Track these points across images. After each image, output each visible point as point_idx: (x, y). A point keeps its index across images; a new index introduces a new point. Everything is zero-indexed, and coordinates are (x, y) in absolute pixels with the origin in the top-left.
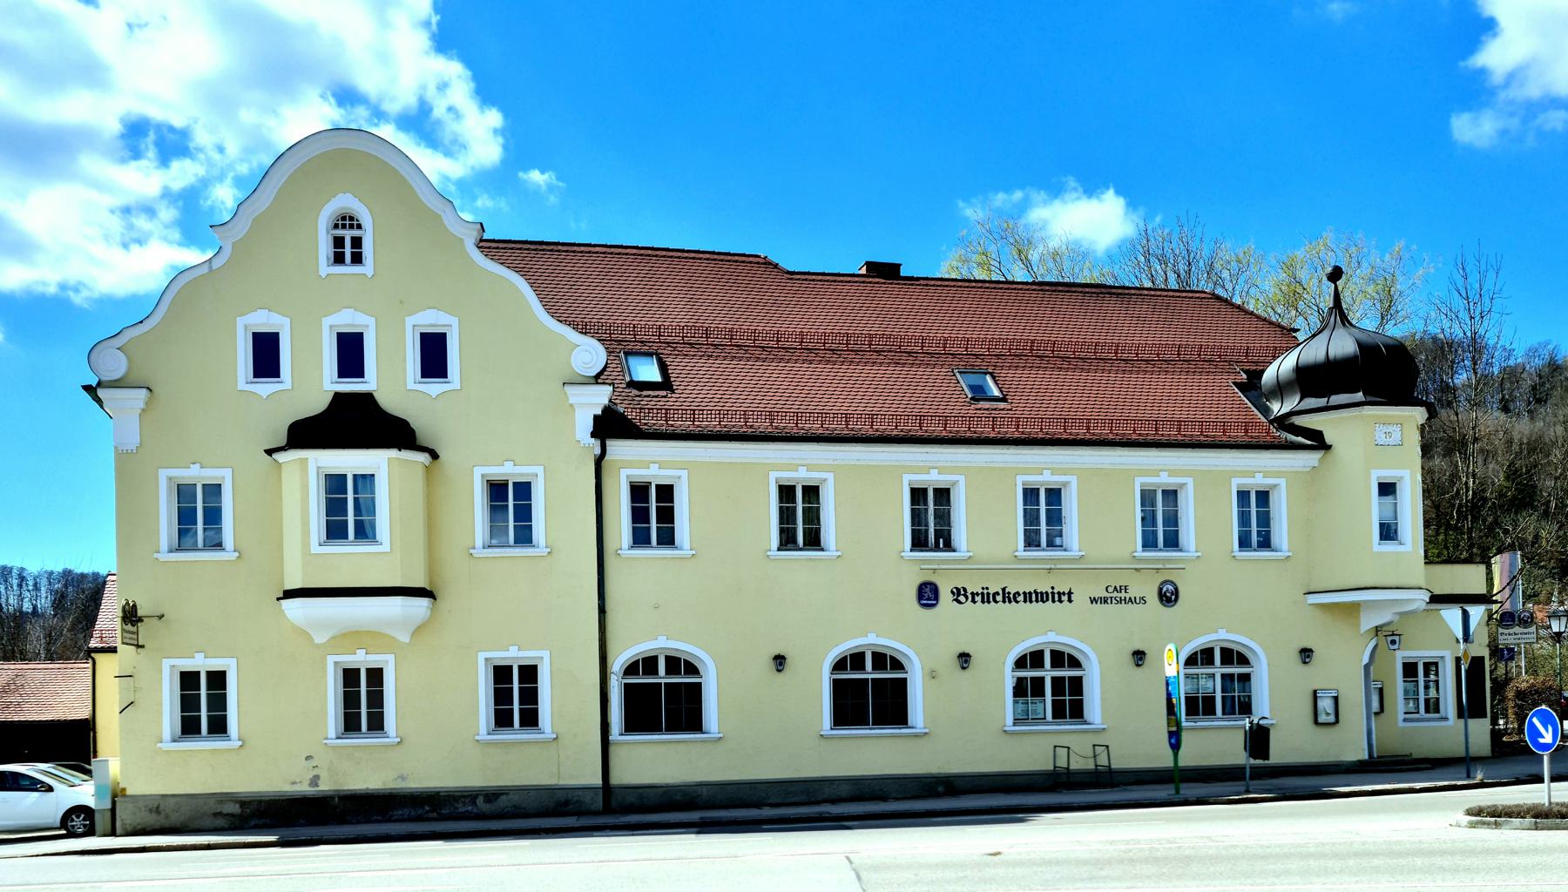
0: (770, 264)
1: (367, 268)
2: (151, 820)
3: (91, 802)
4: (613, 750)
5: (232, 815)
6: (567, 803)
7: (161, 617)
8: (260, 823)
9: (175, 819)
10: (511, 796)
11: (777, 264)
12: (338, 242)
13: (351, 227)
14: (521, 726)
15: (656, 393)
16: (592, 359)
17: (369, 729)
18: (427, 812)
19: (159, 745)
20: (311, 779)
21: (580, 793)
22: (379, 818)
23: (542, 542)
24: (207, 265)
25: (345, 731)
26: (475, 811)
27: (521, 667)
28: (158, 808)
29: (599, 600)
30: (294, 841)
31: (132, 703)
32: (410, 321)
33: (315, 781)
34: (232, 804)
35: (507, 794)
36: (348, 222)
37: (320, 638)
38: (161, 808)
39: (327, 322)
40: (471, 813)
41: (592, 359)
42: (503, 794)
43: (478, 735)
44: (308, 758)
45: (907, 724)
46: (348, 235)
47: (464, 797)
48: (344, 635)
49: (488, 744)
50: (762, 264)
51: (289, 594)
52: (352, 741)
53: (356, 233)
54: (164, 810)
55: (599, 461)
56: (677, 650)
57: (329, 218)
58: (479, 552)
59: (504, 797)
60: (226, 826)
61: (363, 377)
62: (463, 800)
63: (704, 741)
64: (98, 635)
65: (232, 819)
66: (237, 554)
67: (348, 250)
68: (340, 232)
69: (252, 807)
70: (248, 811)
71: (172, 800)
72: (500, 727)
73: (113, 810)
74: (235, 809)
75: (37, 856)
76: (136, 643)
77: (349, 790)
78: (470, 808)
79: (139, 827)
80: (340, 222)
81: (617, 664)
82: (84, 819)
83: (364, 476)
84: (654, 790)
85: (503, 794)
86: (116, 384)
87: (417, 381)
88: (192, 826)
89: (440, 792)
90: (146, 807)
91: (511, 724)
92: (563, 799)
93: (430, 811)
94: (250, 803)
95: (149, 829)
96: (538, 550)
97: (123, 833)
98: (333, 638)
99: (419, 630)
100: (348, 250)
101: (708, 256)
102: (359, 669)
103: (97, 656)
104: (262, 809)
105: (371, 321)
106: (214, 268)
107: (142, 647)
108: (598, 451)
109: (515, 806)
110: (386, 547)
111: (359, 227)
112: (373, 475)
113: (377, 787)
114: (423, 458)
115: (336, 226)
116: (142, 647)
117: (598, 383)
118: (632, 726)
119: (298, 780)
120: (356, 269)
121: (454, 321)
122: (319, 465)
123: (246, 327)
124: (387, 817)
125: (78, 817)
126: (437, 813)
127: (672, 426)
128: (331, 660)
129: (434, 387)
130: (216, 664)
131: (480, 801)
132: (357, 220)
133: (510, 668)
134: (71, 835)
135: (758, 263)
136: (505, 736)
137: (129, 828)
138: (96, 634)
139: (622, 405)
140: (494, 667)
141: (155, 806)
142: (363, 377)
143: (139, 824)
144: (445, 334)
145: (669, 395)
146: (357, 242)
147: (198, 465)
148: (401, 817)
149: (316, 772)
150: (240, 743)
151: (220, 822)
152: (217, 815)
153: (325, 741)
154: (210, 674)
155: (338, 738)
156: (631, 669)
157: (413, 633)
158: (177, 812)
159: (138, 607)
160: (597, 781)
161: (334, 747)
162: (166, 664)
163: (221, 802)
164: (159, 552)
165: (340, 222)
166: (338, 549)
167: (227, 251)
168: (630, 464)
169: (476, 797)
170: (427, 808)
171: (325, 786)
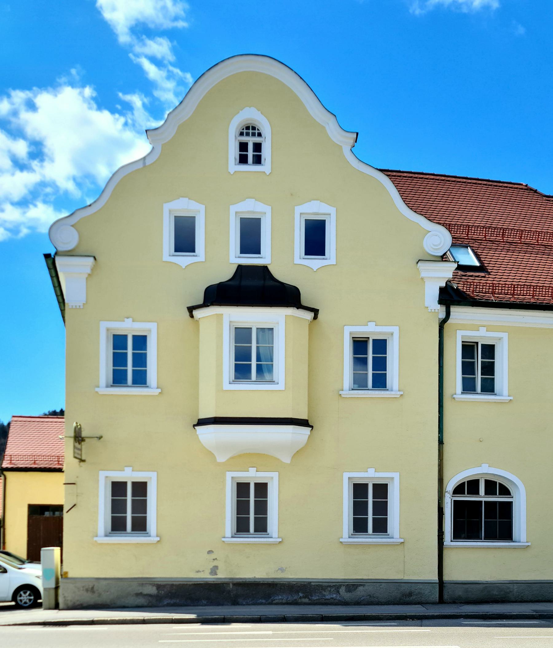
0: (531, 189)
1: (266, 167)
2: (88, 598)
3: (39, 584)
4: (446, 553)
5: (150, 595)
6: (410, 594)
7: (100, 438)
8: (172, 602)
9: (106, 598)
10: (366, 588)
11: (536, 190)
12: (243, 147)
13: (254, 134)
14: (373, 532)
15: (477, 274)
16: (440, 244)
17: (256, 530)
18: (301, 598)
19: (95, 539)
20: (211, 569)
21: (421, 586)
22: (264, 601)
23: (396, 387)
24: (142, 162)
25: (237, 531)
26: (338, 598)
27: (375, 485)
28: (93, 588)
29: (439, 434)
30: (212, 619)
31: (75, 505)
32: (299, 210)
33: (214, 570)
34: (150, 587)
35: (364, 586)
36: (251, 131)
37: (221, 458)
38: (95, 589)
39: (233, 209)
40: (335, 599)
41: (440, 244)
42: (361, 585)
43: (224, 537)
44: (210, 552)
45: (512, 539)
46: (251, 141)
47: (330, 586)
48: (240, 456)
49: (350, 545)
50: (525, 189)
51: (202, 422)
52: (242, 540)
53: (257, 140)
54: (98, 590)
55: (442, 324)
56: (494, 475)
57: (237, 128)
58: (346, 393)
59: (361, 588)
60: (146, 604)
61: (260, 254)
62: (329, 589)
63: (515, 548)
64: (8, 459)
65: (150, 598)
66: (159, 390)
67: (250, 153)
68: (244, 139)
69: (166, 590)
70: (163, 592)
71: (104, 583)
72: (356, 532)
73: (57, 588)
74: (152, 590)
75: (9, 625)
76: (79, 457)
77: (241, 579)
78: (334, 596)
79: (78, 603)
80: (245, 131)
81: (450, 486)
82: (30, 595)
83: (263, 329)
84: (477, 586)
85: (361, 585)
86: (70, 254)
87: (302, 257)
88: (119, 603)
89: (311, 582)
90: (83, 587)
91: (248, 530)
92: (408, 591)
93: (305, 597)
94: (164, 586)
95: (85, 605)
96: (393, 393)
97: (65, 607)
98: (232, 458)
99: (299, 454)
100: (250, 153)
101: (485, 183)
102: (249, 483)
103: (8, 474)
104: (174, 591)
105: (267, 209)
106: (147, 164)
107: (84, 461)
108: (443, 315)
109: (370, 596)
110: (281, 386)
111: (260, 135)
112: (272, 329)
113: (262, 577)
114: (309, 316)
115: (242, 134)
116: (84, 461)
117: (443, 261)
118: (458, 535)
119: (201, 570)
120: (257, 168)
121: (332, 210)
122: (231, 320)
123: (170, 211)
124: (270, 601)
125: (25, 593)
126: (310, 599)
127: (498, 297)
128: (229, 475)
129: (315, 262)
130: (139, 477)
131: (342, 590)
132: (258, 130)
133: (366, 485)
134: (18, 607)
135: (522, 189)
136: (361, 539)
137: (70, 604)
138: (7, 458)
139: (454, 282)
140: (354, 484)
141: (90, 587)
142: (260, 254)
143: (78, 601)
144: (325, 221)
145: (487, 276)
146: (258, 147)
147: (131, 319)
148: (281, 601)
149: (215, 563)
150: (158, 539)
151: (141, 601)
152: (139, 595)
153: (224, 539)
154: (134, 484)
155: (232, 537)
156: (459, 490)
157: (293, 457)
158: (107, 592)
159: (82, 430)
160: (435, 578)
161: (229, 544)
162: (102, 475)
163: (142, 585)
164: (98, 387)
165: (245, 131)
166: (243, 386)
167: (158, 150)
168: (464, 327)
169: (341, 586)
170: (301, 595)
171: (222, 575)
